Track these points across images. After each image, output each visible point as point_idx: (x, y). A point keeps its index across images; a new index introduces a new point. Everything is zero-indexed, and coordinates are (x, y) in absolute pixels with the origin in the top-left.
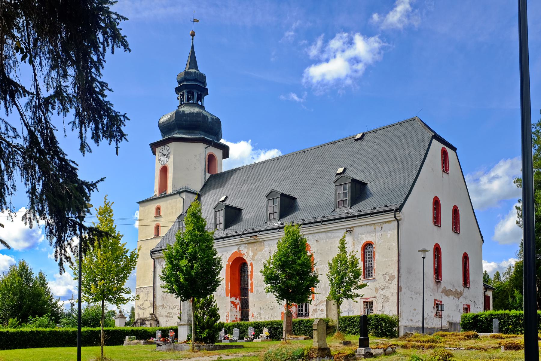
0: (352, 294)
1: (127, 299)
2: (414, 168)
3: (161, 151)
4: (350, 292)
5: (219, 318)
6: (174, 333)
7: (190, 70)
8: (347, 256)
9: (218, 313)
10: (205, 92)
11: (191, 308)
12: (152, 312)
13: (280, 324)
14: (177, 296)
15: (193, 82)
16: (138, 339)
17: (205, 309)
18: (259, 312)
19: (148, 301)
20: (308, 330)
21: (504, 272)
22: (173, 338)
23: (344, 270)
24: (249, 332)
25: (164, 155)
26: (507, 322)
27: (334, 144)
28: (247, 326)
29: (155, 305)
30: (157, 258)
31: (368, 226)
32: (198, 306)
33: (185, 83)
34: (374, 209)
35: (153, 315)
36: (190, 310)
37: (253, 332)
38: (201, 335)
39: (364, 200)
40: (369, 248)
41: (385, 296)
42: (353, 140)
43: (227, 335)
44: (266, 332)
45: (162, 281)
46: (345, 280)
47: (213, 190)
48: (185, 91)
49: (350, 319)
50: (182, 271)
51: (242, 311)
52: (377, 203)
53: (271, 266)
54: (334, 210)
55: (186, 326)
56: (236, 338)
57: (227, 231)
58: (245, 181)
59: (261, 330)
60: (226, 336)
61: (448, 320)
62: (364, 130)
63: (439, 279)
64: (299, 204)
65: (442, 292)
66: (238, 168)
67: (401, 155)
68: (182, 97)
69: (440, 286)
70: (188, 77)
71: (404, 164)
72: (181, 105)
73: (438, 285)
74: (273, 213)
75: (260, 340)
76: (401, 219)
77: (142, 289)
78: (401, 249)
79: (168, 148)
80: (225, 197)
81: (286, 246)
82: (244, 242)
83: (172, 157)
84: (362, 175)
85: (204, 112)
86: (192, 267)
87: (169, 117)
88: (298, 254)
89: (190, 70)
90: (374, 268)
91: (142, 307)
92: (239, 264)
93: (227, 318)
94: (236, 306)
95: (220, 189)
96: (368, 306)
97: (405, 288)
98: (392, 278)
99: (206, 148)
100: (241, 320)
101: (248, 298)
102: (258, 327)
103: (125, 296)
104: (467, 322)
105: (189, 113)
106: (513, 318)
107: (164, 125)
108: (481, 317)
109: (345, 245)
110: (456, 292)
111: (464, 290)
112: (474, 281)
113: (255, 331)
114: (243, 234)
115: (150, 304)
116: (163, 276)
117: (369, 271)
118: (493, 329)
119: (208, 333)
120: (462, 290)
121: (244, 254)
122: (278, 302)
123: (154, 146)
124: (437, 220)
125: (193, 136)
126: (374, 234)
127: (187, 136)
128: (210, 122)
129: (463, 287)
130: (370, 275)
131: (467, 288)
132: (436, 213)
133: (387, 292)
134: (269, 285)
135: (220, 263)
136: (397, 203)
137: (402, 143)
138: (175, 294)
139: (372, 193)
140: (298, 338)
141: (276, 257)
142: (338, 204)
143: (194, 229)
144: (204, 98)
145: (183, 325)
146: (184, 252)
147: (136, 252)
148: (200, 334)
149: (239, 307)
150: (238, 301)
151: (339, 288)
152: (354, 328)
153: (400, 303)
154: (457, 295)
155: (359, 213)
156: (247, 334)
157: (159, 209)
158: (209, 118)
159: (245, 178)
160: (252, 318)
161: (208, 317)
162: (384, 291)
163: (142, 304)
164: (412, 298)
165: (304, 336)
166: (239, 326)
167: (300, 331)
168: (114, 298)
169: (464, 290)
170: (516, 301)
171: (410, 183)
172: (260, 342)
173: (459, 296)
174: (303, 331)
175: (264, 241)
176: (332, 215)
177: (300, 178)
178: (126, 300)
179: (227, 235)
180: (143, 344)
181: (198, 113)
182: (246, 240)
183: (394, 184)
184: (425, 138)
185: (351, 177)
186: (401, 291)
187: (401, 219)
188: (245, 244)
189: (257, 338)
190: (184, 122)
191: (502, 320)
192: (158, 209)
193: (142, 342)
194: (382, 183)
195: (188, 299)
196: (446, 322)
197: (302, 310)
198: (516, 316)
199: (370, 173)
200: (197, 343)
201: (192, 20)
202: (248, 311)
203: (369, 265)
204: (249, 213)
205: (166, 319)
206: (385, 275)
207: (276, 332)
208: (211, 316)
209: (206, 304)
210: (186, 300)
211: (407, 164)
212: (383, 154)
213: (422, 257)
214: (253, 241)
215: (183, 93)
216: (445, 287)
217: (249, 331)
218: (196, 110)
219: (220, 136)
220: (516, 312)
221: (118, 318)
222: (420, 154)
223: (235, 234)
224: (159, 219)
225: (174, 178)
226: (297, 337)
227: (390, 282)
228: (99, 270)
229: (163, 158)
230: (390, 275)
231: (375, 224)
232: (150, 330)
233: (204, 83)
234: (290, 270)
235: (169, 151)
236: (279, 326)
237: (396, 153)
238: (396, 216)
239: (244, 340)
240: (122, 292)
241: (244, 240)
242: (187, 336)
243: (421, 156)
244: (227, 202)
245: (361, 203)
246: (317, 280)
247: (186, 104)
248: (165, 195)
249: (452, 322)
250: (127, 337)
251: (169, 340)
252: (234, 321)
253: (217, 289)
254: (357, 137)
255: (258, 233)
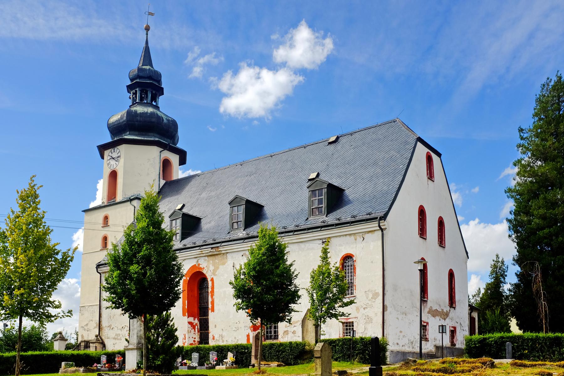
0: (337, 313)
1: (55, 316)
2: (398, 173)
3: (110, 154)
4: (334, 310)
5: (177, 341)
6: (122, 359)
7: (144, 67)
8: (330, 267)
9: (176, 334)
10: (160, 91)
11: (142, 328)
12: (98, 334)
13: (248, 348)
14: (123, 312)
15: (146, 79)
16: (76, 366)
17: (160, 330)
18: (221, 334)
19: (94, 322)
20: (281, 355)
21: (474, 294)
22: (121, 364)
23: (327, 284)
24: (211, 358)
25: (113, 158)
26: (520, 346)
27: (305, 148)
28: (208, 350)
29: (101, 325)
30: (104, 273)
31: (348, 237)
32: (151, 325)
33: (138, 80)
34: (354, 217)
35: (99, 337)
36: (141, 330)
37: (215, 357)
38: (154, 361)
39: (342, 207)
40: (349, 261)
41: (368, 316)
42: (327, 143)
43: (185, 361)
44: (230, 357)
45: (105, 292)
46: (328, 296)
47: (167, 198)
48: (137, 89)
49: (330, 342)
50: (131, 279)
51: (200, 333)
52: (357, 211)
53: (242, 277)
54: (308, 219)
55: (136, 351)
56: (195, 364)
57: (185, 242)
58: (204, 188)
59: (225, 354)
60: (184, 361)
61: (434, 343)
62: (339, 133)
63: (425, 298)
64: (267, 212)
65: (429, 313)
66: (196, 174)
67: (382, 159)
68: (134, 96)
69: (426, 305)
70: (141, 74)
71: (386, 168)
72: (133, 104)
73: (425, 305)
74: (237, 222)
75: (224, 366)
76: (386, 228)
77: (87, 307)
78: (386, 263)
79: (118, 151)
80: (182, 205)
81: (261, 252)
82: (204, 255)
83: (122, 160)
84: (338, 181)
85: (158, 112)
86: (145, 273)
87: (119, 117)
88: (276, 263)
89: (144, 67)
90: (355, 284)
91: (86, 328)
92: (198, 279)
93: (184, 341)
94: (194, 328)
95: (176, 197)
96: (348, 328)
97: (391, 308)
98: (376, 295)
99: (161, 152)
100: (200, 343)
101: (208, 319)
102: (222, 352)
103: (52, 311)
104: (473, 346)
105: (143, 113)
106: (529, 342)
107: (114, 125)
108: (490, 340)
109: (328, 255)
110: (442, 313)
111: (450, 310)
112: (459, 301)
113: (218, 356)
114: (202, 246)
115: (96, 325)
116: (106, 285)
117: (349, 287)
118: (507, 355)
119: (163, 359)
120: (448, 311)
121: (204, 268)
122: (251, 322)
123: (102, 148)
124: (422, 232)
125: (147, 138)
126: (355, 246)
127: (140, 138)
128: (165, 124)
129: (449, 307)
130: (350, 292)
131: (453, 309)
132: (422, 223)
133: (370, 312)
134: (240, 301)
135: (180, 270)
136: (380, 211)
137: (382, 146)
138: (121, 309)
139: (351, 200)
140: (269, 364)
141: (249, 265)
142: (312, 212)
143: (148, 225)
144: (159, 98)
145: (132, 349)
146: (134, 255)
147: (70, 253)
148: (153, 361)
149: (198, 328)
150: (196, 321)
151: (322, 305)
152: (336, 353)
153: (385, 324)
154: (443, 315)
155: (337, 222)
156: (209, 360)
157: (107, 219)
158: (164, 119)
159: (205, 185)
160: (213, 340)
161: (164, 339)
162: (366, 310)
163: (87, 325)
164: (398, 318)
165: (277, 362)
166: (199, 350)
167: (271, 356)
168: (37, 313)
169: (450, 310)
170: (488, 323)
171: (395, 189)
172: (223, 371)
173: (445, 317)
174: (275, 356)
175: (227, 253)
176: (306, 224)
177: (267, 184)
178: (53, 317)
179: (184, 247)
180: (83, 372)
181: (152, 113)
182: (207, 252)
183: (376, 189)
184: (408, 141)
185: (327, 182)
186: (386, 310)
187: (386, 228)
188: (205, 256)
189: (221, 364)
190: (137, 123)
191: (516, 344)
192: (106, 218)
193: (82, 369)
194: (362, 189)
195: (138, 317)
196: (433, 346)
197: (271, 332)
198: (532, 339)
199: (347, 179)
200: (149, 372)
201: (147, 13)
202: (208, 333)
203: (348, 280)
204: (209, 223)
205: (114, 341)
206: (367, 292)
207: (243, 357)
208: (167, 339)
209: (161, 323)
210: (136, 318)
211: (389, 169)
212: (361, 158)
213: (419, 270)
214: (214, 253)
215: (136, 91)
216: (431, 307)
217: (211, 356)
218: (150, 110)
219: (176, 140)
220: (532, 334)
221: (57, 340)
222: (405, 157)
223: (194, 245)
224: (106, 229)
225: (124, 185)
226: (268, 363)
227: (373, 300)
228: (17, 274)
229: (113, 162)
230: (374, 292)
231: (356, 234)
232: (94, 355)
233: (159, 81)
234: (266, 282)
235: (119, 155)
236: (246, 351)
237: (376, 157)
238: (381, 224)
239: (205, 367)
240: (49, 306)
241: (203, 252)
242: (137, 363)
243: (405, 159)
244: (185, 210)
245: (338, 211)
246: (298, 295)
247: (139, 104)
248: (114, 202)
249: (439, 345)
250: (63, 364)
251: (116, 367)
252: (191, 344)
253: (176, 304)
254: (331, 140)
255: (220, 244)
